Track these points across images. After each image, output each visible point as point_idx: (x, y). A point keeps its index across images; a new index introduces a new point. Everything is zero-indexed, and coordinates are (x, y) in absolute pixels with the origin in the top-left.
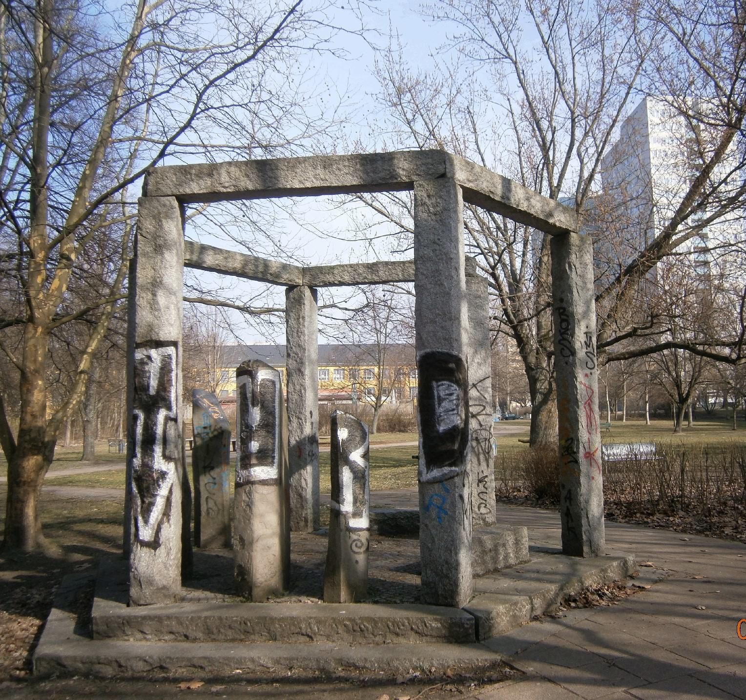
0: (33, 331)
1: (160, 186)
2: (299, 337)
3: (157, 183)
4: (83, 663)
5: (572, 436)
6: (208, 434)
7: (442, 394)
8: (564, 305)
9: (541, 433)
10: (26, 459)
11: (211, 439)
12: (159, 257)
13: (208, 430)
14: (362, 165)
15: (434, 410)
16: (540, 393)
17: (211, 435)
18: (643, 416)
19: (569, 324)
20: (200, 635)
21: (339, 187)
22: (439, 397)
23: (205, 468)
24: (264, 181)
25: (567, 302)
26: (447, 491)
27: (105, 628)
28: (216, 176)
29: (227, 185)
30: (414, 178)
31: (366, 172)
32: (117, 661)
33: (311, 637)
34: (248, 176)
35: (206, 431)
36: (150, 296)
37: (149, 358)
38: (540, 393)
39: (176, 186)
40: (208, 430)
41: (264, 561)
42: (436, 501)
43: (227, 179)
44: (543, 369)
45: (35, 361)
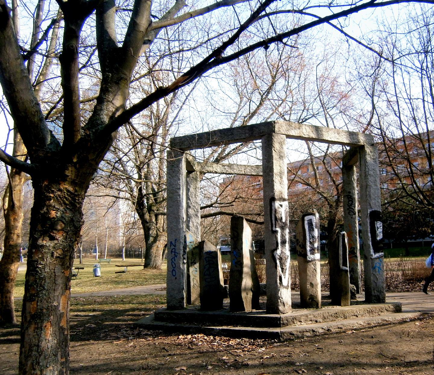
0: (18, 181)
1: (280, 129)
2: (196, 198)
3: (279, 128)
4: (300, 332)
5: (353, 246)
6: (192, 246)
7: (378, 226)
8: (351, 194)
9: (153, 259)
10: (13, 264)
11: (194, 248)
12: (282, 161)
13: (192, 244)
14: (349, 135)
15: (376, 232)
16: (152, 236)
17: (194, 246)
18: (120, 256)
19: (353, 202)
20: (321, 320)
21: (293, 136)
22: (377, 227)
23: (192, 263)
24: (318, 135)
25: (353, 193)
26: (381, 261)
27: (286, 322)
28: (301, 129)
29: (305, 134)
30: (365, 144)
31: (350, 138)
32: (312, 330)
33: (357, 316)
34: (313, 132)
35: (191, 244)
36: (279, 178)
37: (281, 206)
38: (152, 236)
39: (286, 130)
40: (192, 244)
41: (319, 293)
42: (378, 265)
43: (305, 132)
44: (153, 223)
45: (19, 200)
